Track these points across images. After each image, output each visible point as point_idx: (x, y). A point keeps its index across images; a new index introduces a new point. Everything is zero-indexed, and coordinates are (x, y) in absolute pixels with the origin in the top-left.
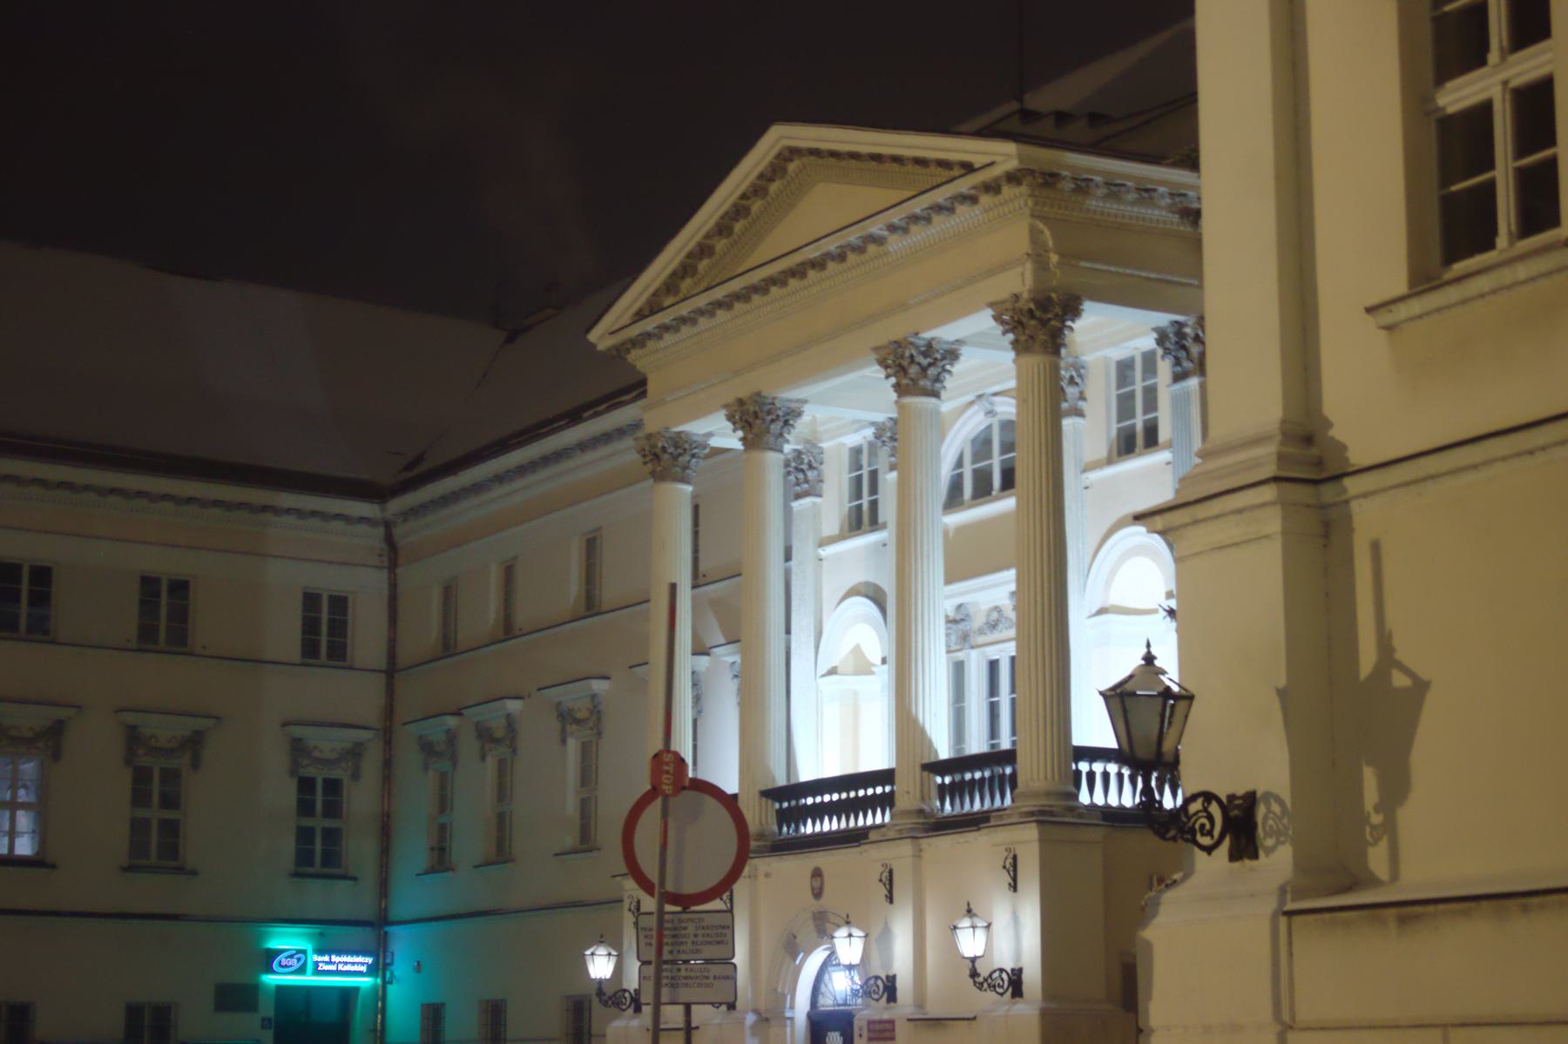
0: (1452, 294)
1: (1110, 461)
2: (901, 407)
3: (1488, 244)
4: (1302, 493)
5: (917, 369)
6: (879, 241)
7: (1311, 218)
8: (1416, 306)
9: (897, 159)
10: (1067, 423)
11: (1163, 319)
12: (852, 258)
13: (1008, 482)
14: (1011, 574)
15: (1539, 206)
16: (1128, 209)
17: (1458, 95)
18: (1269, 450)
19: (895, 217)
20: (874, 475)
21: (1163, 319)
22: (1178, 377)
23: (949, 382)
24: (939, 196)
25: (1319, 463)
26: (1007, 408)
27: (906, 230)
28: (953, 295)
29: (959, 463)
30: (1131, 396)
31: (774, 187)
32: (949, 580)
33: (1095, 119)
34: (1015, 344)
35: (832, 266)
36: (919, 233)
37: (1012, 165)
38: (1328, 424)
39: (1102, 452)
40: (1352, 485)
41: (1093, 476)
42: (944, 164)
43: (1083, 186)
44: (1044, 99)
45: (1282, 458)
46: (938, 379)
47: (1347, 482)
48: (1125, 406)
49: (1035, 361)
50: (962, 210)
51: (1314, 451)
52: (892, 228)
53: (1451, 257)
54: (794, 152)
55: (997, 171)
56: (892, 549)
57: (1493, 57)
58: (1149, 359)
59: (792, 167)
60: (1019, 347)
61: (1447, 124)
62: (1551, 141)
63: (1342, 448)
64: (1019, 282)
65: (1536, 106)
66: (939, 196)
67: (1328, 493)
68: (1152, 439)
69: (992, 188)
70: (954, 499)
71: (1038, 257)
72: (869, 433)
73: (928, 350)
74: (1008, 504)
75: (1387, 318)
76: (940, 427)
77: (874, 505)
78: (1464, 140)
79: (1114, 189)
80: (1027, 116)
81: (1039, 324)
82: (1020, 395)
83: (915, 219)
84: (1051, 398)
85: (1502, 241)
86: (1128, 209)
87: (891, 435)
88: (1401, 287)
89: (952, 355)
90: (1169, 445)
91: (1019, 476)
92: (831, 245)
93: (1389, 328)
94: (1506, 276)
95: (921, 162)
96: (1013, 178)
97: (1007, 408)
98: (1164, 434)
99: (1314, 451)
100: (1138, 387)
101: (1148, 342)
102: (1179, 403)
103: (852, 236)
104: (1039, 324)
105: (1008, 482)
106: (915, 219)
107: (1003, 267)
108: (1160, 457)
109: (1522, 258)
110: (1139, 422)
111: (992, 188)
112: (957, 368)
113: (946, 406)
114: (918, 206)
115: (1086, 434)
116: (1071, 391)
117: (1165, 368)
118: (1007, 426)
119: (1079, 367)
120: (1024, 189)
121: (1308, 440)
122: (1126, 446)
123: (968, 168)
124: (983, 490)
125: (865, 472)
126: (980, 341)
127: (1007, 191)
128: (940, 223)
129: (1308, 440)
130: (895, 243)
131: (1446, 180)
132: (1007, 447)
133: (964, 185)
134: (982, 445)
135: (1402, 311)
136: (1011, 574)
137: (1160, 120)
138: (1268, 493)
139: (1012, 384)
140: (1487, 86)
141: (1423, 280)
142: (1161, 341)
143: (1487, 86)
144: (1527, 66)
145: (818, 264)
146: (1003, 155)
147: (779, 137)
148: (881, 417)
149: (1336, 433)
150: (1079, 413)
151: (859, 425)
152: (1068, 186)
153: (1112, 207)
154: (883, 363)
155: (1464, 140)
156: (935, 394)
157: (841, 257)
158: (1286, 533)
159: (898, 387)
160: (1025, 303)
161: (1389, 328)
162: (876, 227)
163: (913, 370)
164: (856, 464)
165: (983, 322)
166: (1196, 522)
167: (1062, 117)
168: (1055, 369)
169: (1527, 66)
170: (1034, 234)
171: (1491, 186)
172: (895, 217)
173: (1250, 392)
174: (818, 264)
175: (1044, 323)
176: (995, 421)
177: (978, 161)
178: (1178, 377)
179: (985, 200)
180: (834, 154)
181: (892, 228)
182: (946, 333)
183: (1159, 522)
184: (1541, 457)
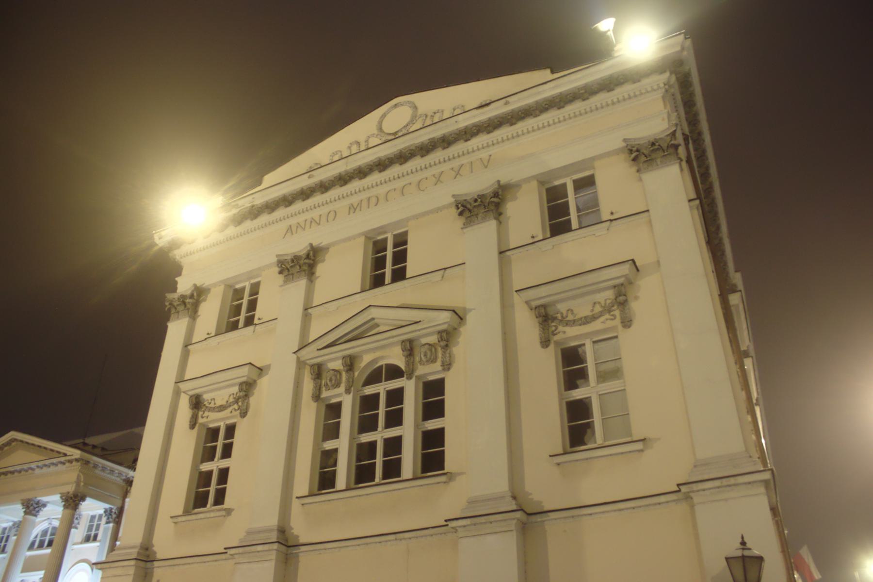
0: (194, 517)
1: (81, 543)
2: (24, 518)
3: (205, 506)
4: (142, 564)
5: (32, 508)
6: (33, 469)
7: (281, 507)
8: (184, 518)
9: (45, 448)
10: (73, 530)
11: (107, 506)
12: (23, 473)
13: (50, 544)
14: (43, 572)
15: (220, 498)
16: (106, 475)
17: (206, 467)
18: (136, 550)
19: (40, 464)
20: (8, 537)
21: (107, 506)
22: (107, 523)
23: (41, 513)
24: (54, 461)
25: (148, 556)
26: (56, 523)
27: (42, 468)
28: (49, 489)
29: (36, 537)
30: (92, 526)
31: (6, 448)
32: (22, 571)
33: (103, 449)
34: (64, 506)
35: (16, 474)
36: (45, 470)
37: (78, 456)
38: (153, 546)
39: (80, 540)
40: (156, 564)
41: (75, 547)
42: (58, 452)
43: (95, 466)
44: (91, 440)
45: (139, 553)
46: (38, 512)
47: (155, 563)
48: (90, 528)
49: (69, 511)
50: (60, 466)
51: (148, 553)
52: (38, 467)
53: (195, 507)
54: (15, 440)
55: (73, 457)
56: (6, 562)
57: (216, 459)
58: (100, 516)
59: (13, 444)
60: (65, 507)
61: (201, 473)
62: (226, 483)
63: (155, 553)
64: (70, 489)
65: (224, 474)
66: (54, 461)
67: (149, 565)
68: (95, 538)
69: (70, 462)
70: (31, 547)
71: (78, 483)
72: (11, 524)
73: (38, 503)
74: (49, 551)
75: (175, 520)
76: (34, 525)
77: (5, 546)
78: (205, 478)
79: (104, 469)
80: (85, 444)
81: (73, 502)
82: (62, 520)
83: (45, 465)
84: (69, 523)
85: (208, 506)
86: (106, 475)
87: (18, 526)
88: (181, 513)
89: (44, 505)
90: (100, 541)
91: (54, 544)
92: (18, 468)
93: (175, 523)
94: (208, 515)
95: (52, 450)
96: (77, 460)
97: (56, 523)
98: (99, 538)
99: (148, 553)
100: (95, 523)
101: (102, 512)
102: (106, 530)
103: (25, 467)
104: (73, 502)
105: (50, 544)
106: (45, 465)
107: (67, 484)
108: (96, 544)
109: (213, 511)
110: (93, 533)
111: (70, 462)
112: (45, 509)
113: (38, 519)
114: (47, 462)
115: (77, 534)
116: (76, 521)
117: (104, 519)
118: (54, 528)
119: (80, 515)
120: (79, 464)
121: (147, 549)
122: (87, 539)
123: (65, 455)
124: (41, 546)
125: (5, 535)
126: (54, 503)
127: (74, 463)
128: (52, 468)
129: (147, 549)
130: (38, 471)
131: (198, 487)
132: (52, 534)
133: (63, 459)
134: (45, 533)
135: (180, 519)
136: (43, 572)
137: (127, 453)
138: (133, 562)
139: (60, 516)
140: (214, 466)
141: (187, 512)
142: (106, 511)
143: (214, 466)
144: (224, 464)
145: (12, 473)
146: (76, 453)
147: (13, 434)
148: (16, 520)
149: (155, 549)
150: (76, 528)
151: (8, 521)
152: (91, 465)
153: (102, 474)
154: (23, 504)
155: (205, 478)
156: (36, 516)
157: (20, 472)
158: (134, 574)
159: (25, 512)
160: (71, 495)
161: (175, 523)
162: (33, 466)
163: (31, 508)
164: (3, 533)
165: (57, 498)
166: (110, 568)
167: (94, 447)
168: (73, 515)
169: (224, 464)
170: (78, 476)
171: (208, 492)
172: (40, 464)
173: (132, 532)
174: (12, 473)
175: (74, 501)
176: (51, 527)
177: (68, 453)
178: (107, 523)
179: (67, 464)
180: (27, 443)
181: (38, 467)
182: (44, 499)
183: (99, 566)
184: (207, 564)
